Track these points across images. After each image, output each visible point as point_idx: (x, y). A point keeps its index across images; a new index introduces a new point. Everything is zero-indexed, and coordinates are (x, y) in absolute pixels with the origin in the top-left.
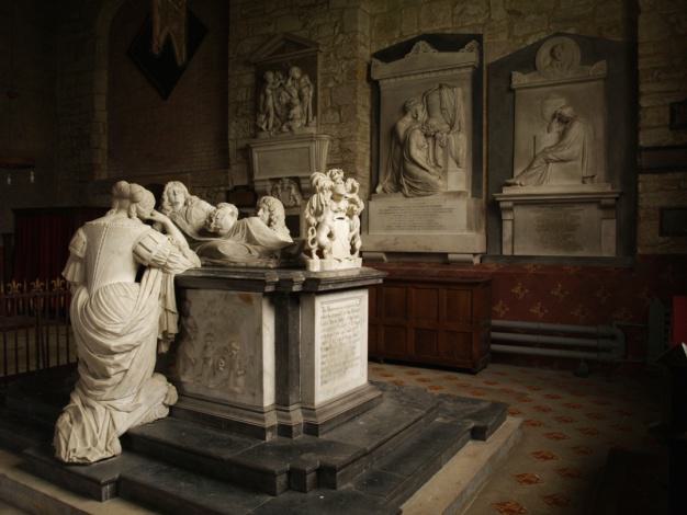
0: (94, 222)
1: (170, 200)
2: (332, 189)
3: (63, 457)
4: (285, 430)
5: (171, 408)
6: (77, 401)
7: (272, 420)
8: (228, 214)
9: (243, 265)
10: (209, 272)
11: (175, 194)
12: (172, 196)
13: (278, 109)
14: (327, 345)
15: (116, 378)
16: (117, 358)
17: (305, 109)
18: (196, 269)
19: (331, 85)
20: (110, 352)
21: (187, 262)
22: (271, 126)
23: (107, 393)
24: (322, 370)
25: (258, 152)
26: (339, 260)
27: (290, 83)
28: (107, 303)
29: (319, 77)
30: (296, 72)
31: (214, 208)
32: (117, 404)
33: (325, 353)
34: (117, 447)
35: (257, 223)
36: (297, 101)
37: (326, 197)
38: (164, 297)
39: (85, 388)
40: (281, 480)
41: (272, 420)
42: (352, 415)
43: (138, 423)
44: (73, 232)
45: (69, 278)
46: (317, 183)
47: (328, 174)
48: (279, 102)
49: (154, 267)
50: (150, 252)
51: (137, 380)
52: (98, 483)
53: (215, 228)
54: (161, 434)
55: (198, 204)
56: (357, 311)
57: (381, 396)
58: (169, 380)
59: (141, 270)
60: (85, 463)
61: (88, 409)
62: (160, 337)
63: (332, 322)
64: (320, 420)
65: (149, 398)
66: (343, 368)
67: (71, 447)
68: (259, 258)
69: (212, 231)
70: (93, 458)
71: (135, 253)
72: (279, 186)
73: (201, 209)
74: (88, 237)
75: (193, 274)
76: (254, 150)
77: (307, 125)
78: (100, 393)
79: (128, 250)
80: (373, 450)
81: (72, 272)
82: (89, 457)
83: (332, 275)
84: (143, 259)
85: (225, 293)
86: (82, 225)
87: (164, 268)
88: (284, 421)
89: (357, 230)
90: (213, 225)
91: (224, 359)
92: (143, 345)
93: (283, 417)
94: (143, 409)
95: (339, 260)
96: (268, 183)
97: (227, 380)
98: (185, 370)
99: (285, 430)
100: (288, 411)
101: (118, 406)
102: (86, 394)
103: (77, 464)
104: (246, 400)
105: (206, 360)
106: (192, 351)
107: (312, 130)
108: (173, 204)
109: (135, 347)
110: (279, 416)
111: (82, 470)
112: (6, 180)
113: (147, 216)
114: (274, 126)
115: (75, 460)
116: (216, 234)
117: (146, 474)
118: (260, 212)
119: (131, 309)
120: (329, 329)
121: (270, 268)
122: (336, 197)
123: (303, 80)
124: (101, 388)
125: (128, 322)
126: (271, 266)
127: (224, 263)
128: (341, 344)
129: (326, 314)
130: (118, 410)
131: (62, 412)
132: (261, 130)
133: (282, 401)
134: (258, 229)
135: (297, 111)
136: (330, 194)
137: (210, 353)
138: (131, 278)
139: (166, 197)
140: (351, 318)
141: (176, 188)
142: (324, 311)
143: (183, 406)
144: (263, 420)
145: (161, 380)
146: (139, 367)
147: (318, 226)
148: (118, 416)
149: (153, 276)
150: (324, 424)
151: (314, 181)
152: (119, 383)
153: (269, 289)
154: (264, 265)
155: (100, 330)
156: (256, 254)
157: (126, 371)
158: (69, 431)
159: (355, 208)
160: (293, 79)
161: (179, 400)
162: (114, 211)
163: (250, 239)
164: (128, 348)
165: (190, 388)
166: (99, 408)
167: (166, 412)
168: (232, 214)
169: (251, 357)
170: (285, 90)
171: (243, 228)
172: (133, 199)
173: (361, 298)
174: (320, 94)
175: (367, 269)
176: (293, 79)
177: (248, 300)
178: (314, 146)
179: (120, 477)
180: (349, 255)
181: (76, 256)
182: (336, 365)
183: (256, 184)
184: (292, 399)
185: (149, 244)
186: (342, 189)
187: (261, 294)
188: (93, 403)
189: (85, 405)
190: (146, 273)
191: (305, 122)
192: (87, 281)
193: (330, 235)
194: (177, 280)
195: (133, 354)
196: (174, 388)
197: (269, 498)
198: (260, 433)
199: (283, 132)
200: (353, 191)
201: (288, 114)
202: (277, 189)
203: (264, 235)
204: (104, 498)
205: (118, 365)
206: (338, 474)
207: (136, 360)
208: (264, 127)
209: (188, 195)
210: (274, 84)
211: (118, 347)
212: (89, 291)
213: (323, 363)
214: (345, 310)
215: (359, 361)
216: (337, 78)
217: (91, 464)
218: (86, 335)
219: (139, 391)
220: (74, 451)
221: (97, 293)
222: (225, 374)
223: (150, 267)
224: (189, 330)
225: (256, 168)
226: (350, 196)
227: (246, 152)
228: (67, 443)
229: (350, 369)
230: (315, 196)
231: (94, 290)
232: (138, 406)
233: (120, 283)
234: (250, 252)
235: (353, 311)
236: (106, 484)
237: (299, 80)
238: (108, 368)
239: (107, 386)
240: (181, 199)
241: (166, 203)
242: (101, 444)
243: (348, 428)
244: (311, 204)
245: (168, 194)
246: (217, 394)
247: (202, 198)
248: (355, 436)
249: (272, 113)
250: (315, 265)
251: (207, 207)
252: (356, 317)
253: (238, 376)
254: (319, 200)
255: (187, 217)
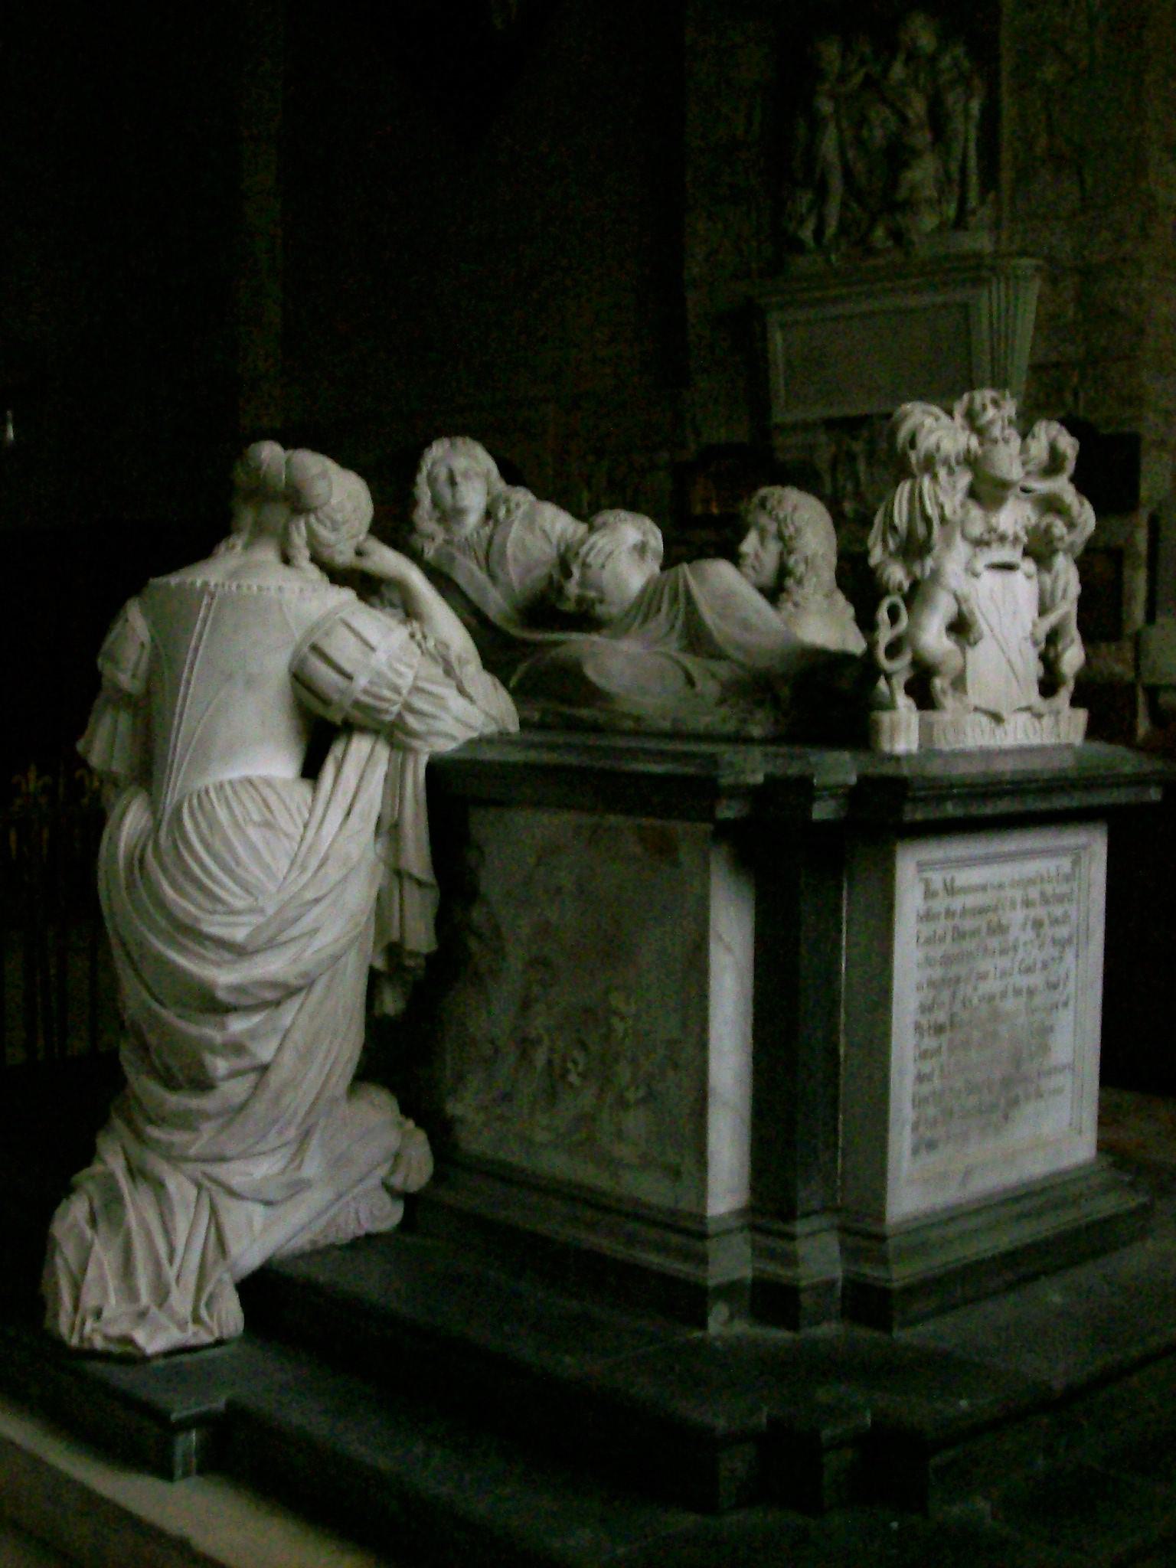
0: (174, 580)
1: (436, 503)
2: (970, 461)
3: (64, 1327)
4: (773, 1300)
5: (411, 1201)
6: (112, 1159)
7: (732, 1262)
8: (625, 552)
9: (666, 725)
10: (552, 747)
11: (452, 482)
12: (446, 492)
13: (860, 167)
14: (941, 1016)
15: (235, 1090)
16: (237, 1025)
17: (954, 168)
18: (502, 738)
19: (1050, 72)
20: (212, 1005)
21: (468, 709)
22: (831, 230)
23: (201, 1141)
24: (919, 1102)
25: (783, 326)
26: (997, 718)
27: (898, 71)
28: (207, 847)
29: (1005, 43)
30: (923, 34)
31: (582, 528)
32: (235, 1174)
33: (929, 1042)
34: (230, 1315)
35: (724, 586)
36: (922, 138)
37: (946, 494)
38: (389, 829)
39: (140, 1121)
40: (735, 1465)
41: (732, 1262)
42: (1020, 1267)
43: (302, 1242)
44: (109, 612)
45: (95, 760)
46: (912, 443)
47: (959, 408)
48: (859, 142)
49: (363, 730)
50: (349, 677)
51: (298, 1101)
52: (159, 1416)
53: (581, 600)
54: (371, 1283)
55: (530, 520)
56: (1060, 899)
57: (1144, 1211)
58: (407, 1110)
59: (320, 733)
60: (130, 1357)
61: (143, 1187)
62: (380, 964)
63: (959, 935)
64: (901, 1273)
65: (338, 1162)
66: (1009, 1091)
67: (90, 1300)
68: (721, 702)
69: (569, 606)
70: (152, 1341)
71: (300, 680)
72: (858, 447)
73: (542, 527)
74: (155, 624)
75: (490, 754)
76: (773, 317)
77: (960, 223)
78: (178, 1137)
79: (276, 666)
80: (1073, 1393)
81: (105, 743)
82: (140, 1337)
83: (962, 769)
84: (326, 702)
85: (587, 820)
86: (135, 587)
87: (393, 734)
88: (773, 1269)
89: (1067, 607)
90: (572, 588)
91: (583, 1046)
92: (319, 989)
93: (772, 1255)
94: (316, 1199)
95: (997, 718)
96: (823, 438)
97: (586, 1119)
98: (460, 1078)
99: (773, 1300)
100: (792, 1237)
101: (236, 1181)
102: (139, 1136)
103: (105, 1356)
104: (650, 1189)
105: (526, 1045)
106: (488, 1015)
107: (980, 241)
108: (448, 515)
109: (298, 990)
110: (759, 1252)
111: (122, 1378)
112: (5, 431)
113: (343, 556)
114: (843, 230)
115: (99, 1343)
116: (586, 619)
117: (298, 1405)
118: (750, 544)
119: (284, 864)
120: (947, 960)
121: (749, 740)
122: (987, 491)
123: (946, 62)
124: (187, 1121)
125: (270, 911)
126: (756, 731)
127: (602, 718)
128: (996, 1016)
129: (940, 904)
130: (232, 1193)
131: (65, 1190)
132: (799, 247)
133: (773, 1199)
134: (726, 600)
135: (923, 173)
136: (964, 479)
137: (540, 1022)
138: (280, 764)
139: (424, 493)
140: (1038, 924)
141: (460, 464)
142: (929, 894)
143: (447, 1196)
144: (702, 1260)
145: (379, 1111)
146: (306, 1055)
147: (916, 594)
148: (234, 1215)
149: (360, 761)
150: (908, 1291)
151: (903, 435)
152: (242, 1107)
153: (727, 811)
154: (730, 727)
155: (188, 932)
156: (709, 688)
157: (264, 1069)
158: (86, 1250)
159: (1059, 528)
160: (911, 57)
161: (438, 1177)
162: (238, 541)
163: (696, 638)
164: (269, 995)
165: (478, 1139)
166: (177, 1185)
167: (388, 1216)
168: (641, 549)
169: (671, 1043)
170: (884, 100)
171: (675, 598)
172: (297, 501)
173: (1077, 856)
174: (1008, 107)
175: (1100, 748)
176: (911, 57)
177: (664, 848)
178: (987, 302)
179: (229, 1404)
180: (1034, 697)
181: (119, 690)
182: (971, 1088)
183: (779, 441)
184: (808, 1194)
185: (344, 649)
186: (1008, 461)
187: (709, 827)
188: (161, 1167)
189: (136, 1172)
190: (337, 749)
191: (951, 211)
192: (148, 771)
193: (960, 627)
194: (438, 772)
195: (288, 1013)
196: (421, 1136)
197: (688, 1520)
198: (689, 1302)
199: (870, 251)
200: (1053, 465)
201: (893, 184)
202: (852, 458)
203: (746, 626)
204: (179, 1472)
205: (237, 1048)
206: (935, 1461)
207: (297, 1036)
208: (807, 234)
209: (500, 486)
210: (842, 78)
211: (239, 989)
212: (154, 806)
213: (921, 1078)
214: (1018, 895)
215: (1064, 1080)
216: (1069, 46)
217: (145, 1359)
218: (142, 944)
219: (306, 1135)
220: (98, 1314)
221: (178, 810)
222: (587, 1099)
223: (349, 728)
224: (473, 944)
225: (778, 381)
226: (1042, 486)
227: (744, 327)
228: (77, 1287)
229: (1029, 1108)
230: (905, 488)
231: (170, 800)
232: (297, 1187)
233: (250, 782)
234: (690, 681)
235: (1045, 900)
236: (184, 1426)
237: (933, 59)
238: (209, 1059)
239: (207, 1116)
240: (473, 498)
241: (424, 515)
242: (181, 1301)
243: (1005, 1309)
244: (889, 514)
245: (432, 481)
246: (557, 1164)
247: (543, 494)
248: (1039, 1338)
249: (836, 182)
250: (902, 731)
251: (558, 522)
252: (1064, 920)
253: (622, 1103)
254: (916, 499)
255: (490, 558)
